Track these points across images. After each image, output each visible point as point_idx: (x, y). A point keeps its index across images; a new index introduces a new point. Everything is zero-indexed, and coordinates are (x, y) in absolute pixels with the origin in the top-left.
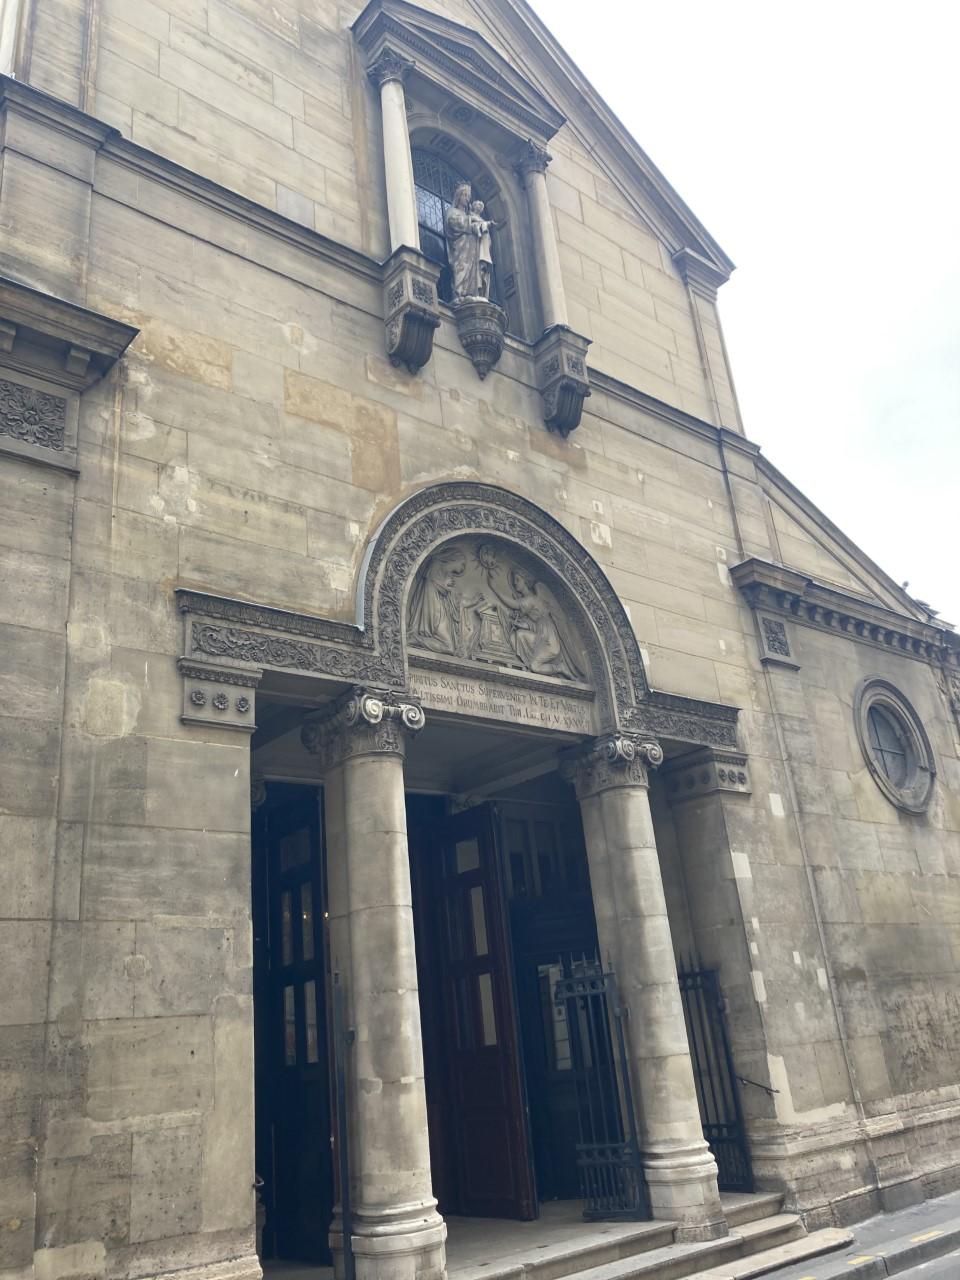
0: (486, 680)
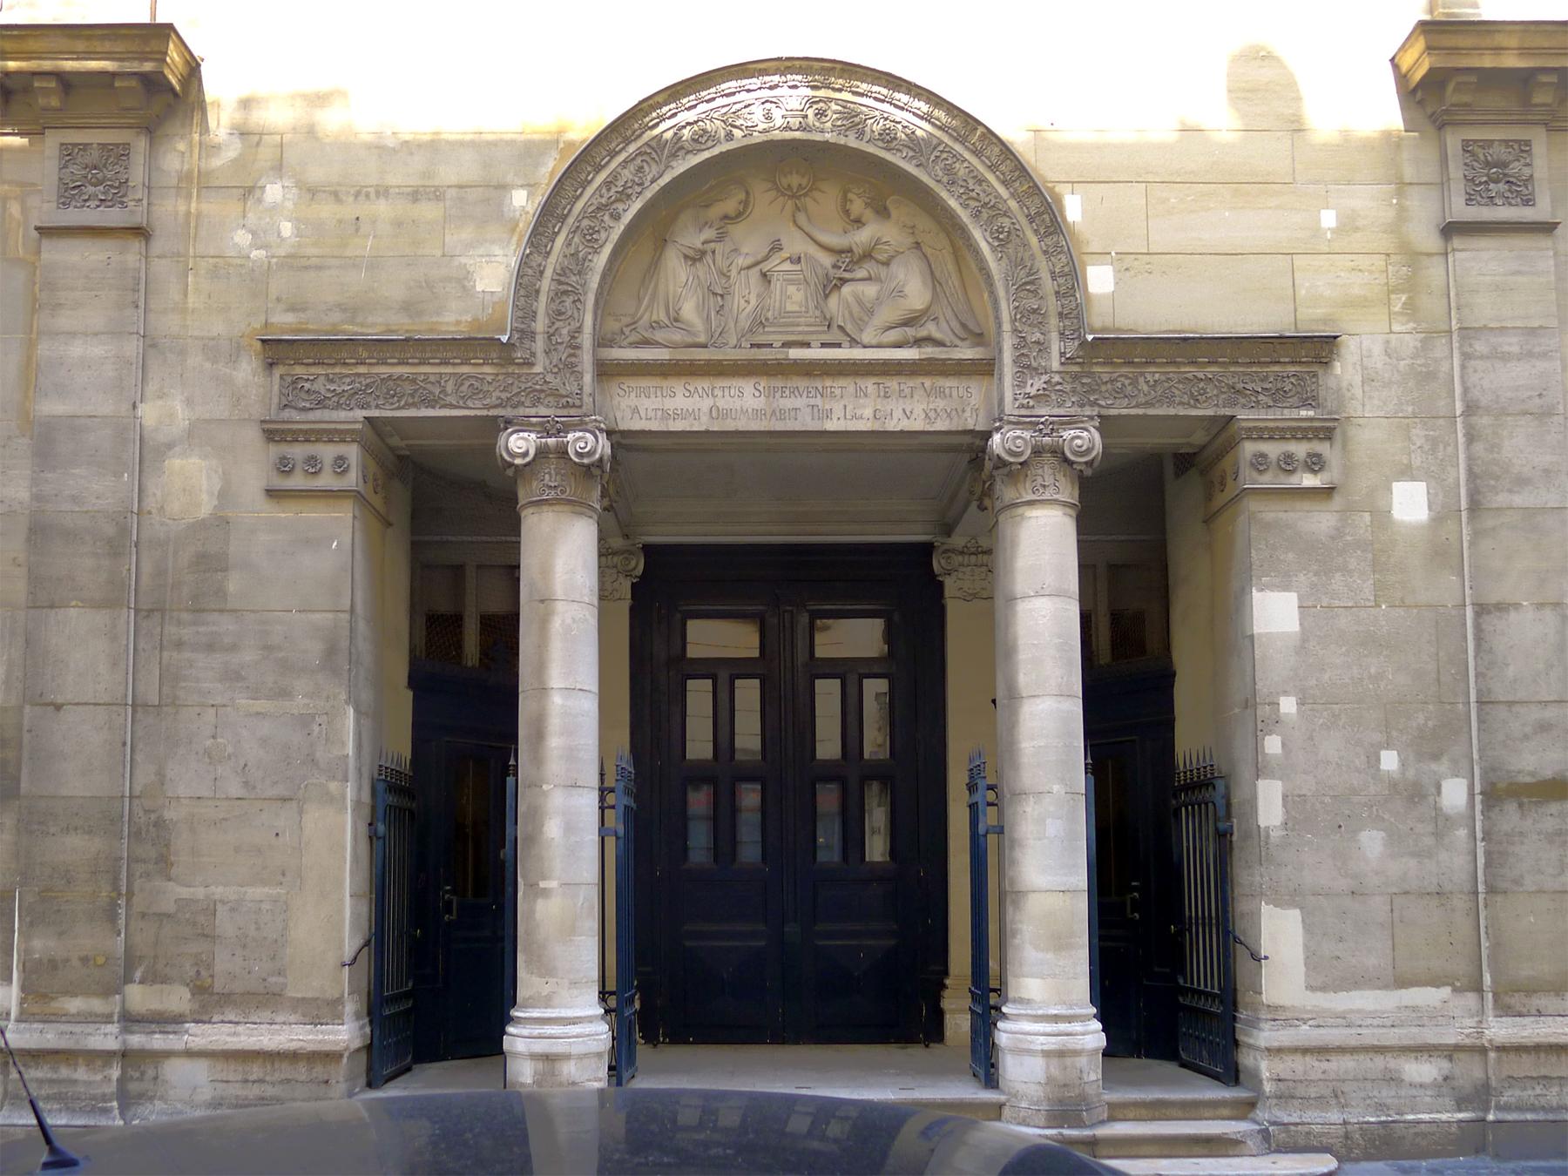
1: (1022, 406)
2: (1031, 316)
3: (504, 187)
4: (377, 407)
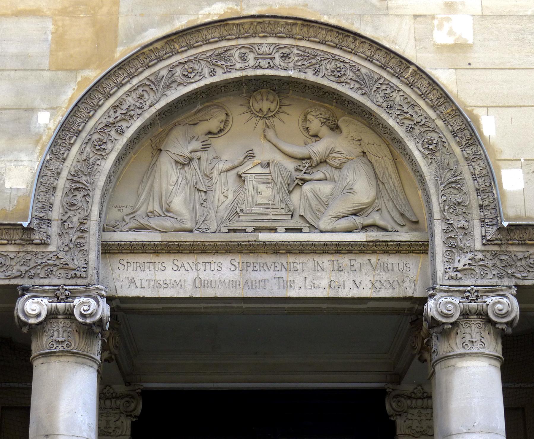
0: (241, 252)
3: (32, 110)
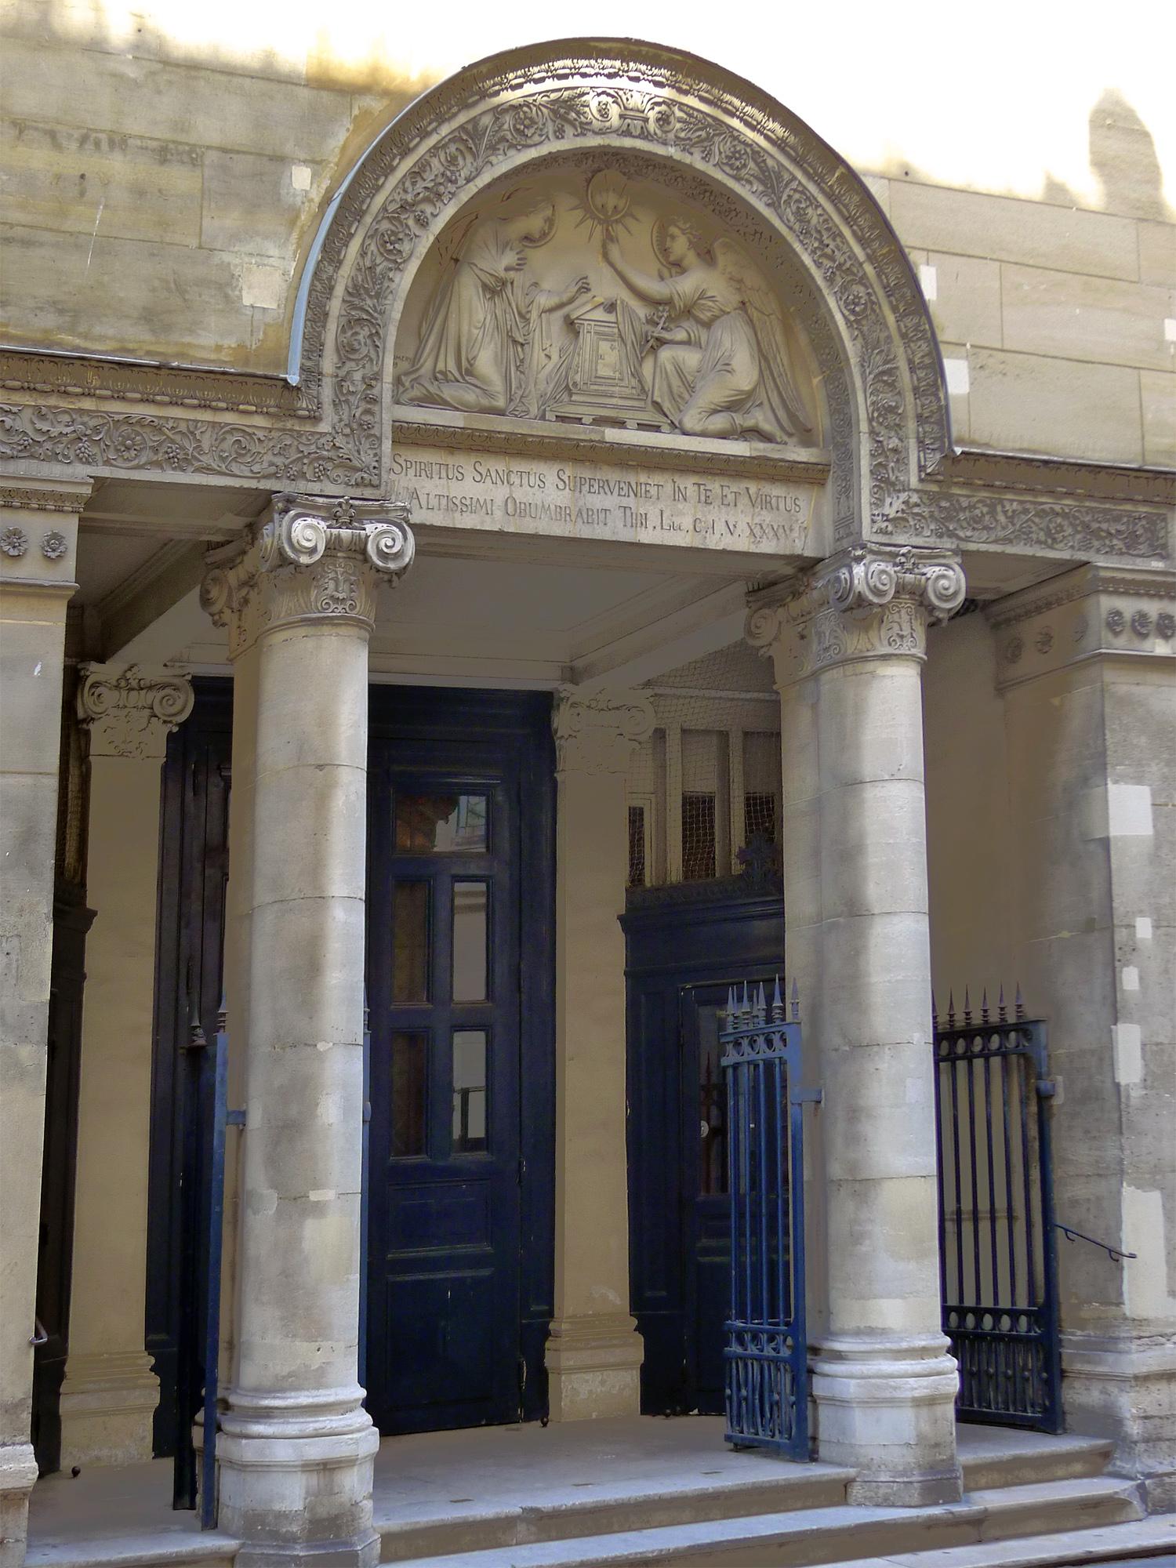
1: (881, 531)
2: (886, 416)
3: (281, 160)
4: (107, 463)
